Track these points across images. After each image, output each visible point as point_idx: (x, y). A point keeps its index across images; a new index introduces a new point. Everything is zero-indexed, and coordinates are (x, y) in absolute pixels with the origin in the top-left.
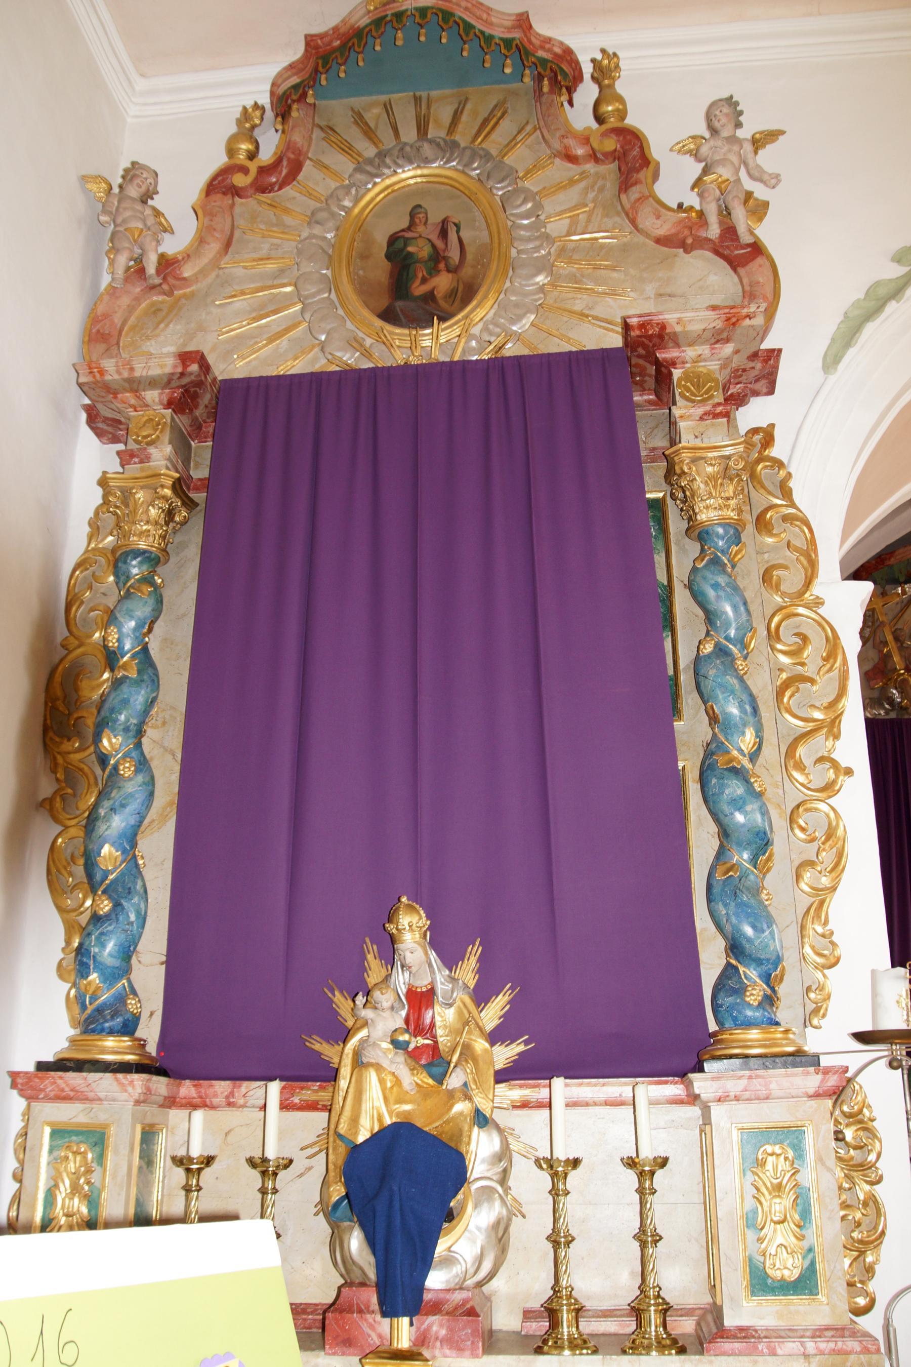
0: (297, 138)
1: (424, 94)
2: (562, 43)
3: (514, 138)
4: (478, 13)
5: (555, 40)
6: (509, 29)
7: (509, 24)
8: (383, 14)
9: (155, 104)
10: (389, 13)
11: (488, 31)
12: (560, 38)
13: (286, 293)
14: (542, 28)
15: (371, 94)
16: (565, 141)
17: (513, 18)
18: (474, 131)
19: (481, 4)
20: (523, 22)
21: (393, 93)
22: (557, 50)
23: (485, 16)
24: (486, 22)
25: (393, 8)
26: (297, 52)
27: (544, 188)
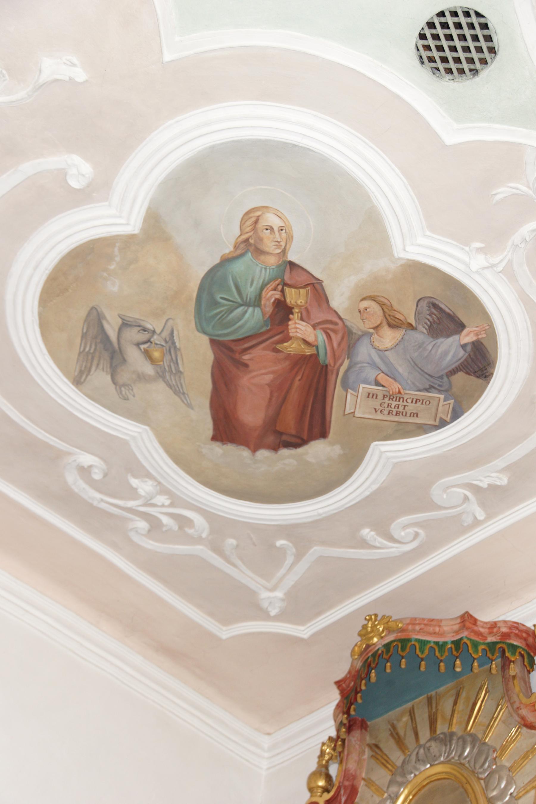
0: (352, 765)
1: (433, 693)
2: (505, 622)
3: (527, 687)
4: (431, 629)
5: (499, 621)
6: (457, 632)
7: (456, 627)
8: (367, 657)
9: (288, 749)
10: (370, 654)
11: (441, 640)
12: (501, 618)
13: (508, 801)
14: (486, 616)
15: (400, 705)
16: (520, 712)
17: (459, 621)
18: (466, 718)
19: (432, 620)
20: (467, 620)
21: (414, 699)
22: (504, 630)
23: (437, 629)
24: (438, 634)
25: (371, 651)
26: (335, 697)
27: (514, 763)
